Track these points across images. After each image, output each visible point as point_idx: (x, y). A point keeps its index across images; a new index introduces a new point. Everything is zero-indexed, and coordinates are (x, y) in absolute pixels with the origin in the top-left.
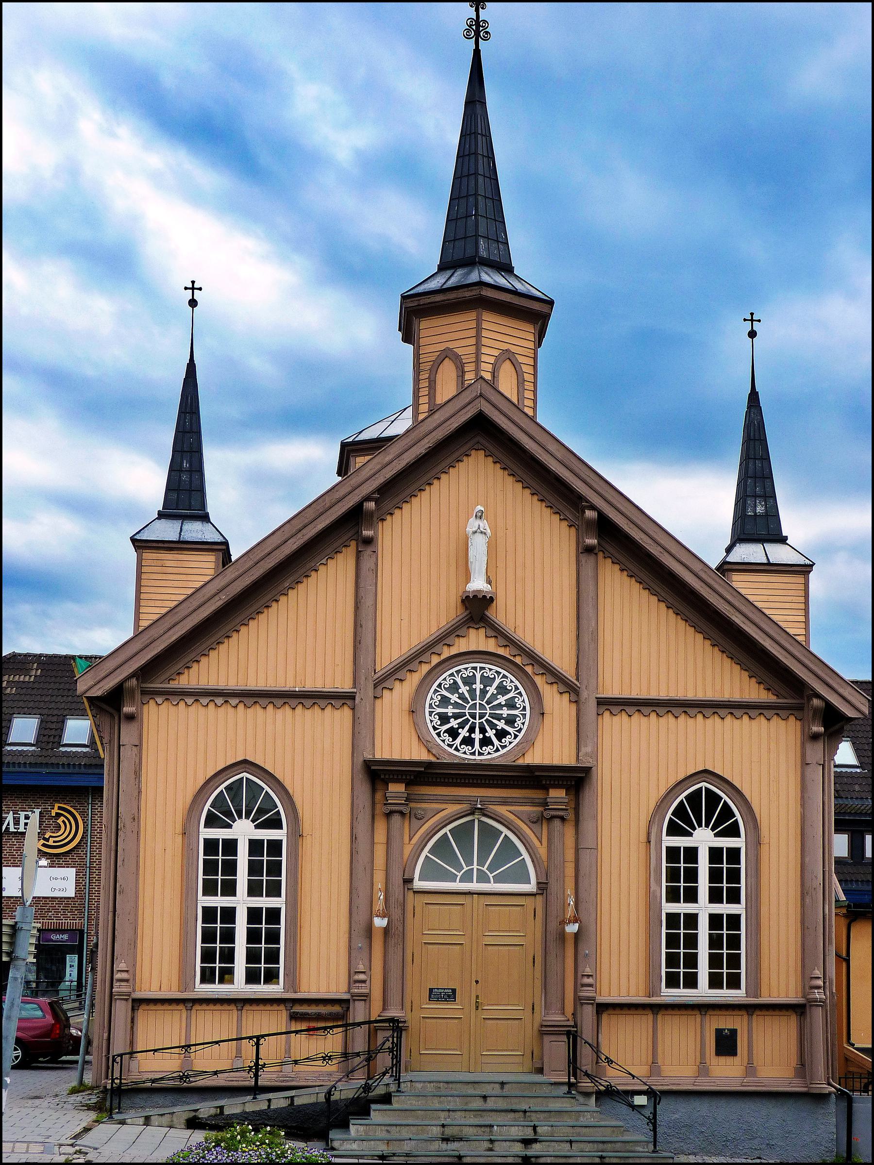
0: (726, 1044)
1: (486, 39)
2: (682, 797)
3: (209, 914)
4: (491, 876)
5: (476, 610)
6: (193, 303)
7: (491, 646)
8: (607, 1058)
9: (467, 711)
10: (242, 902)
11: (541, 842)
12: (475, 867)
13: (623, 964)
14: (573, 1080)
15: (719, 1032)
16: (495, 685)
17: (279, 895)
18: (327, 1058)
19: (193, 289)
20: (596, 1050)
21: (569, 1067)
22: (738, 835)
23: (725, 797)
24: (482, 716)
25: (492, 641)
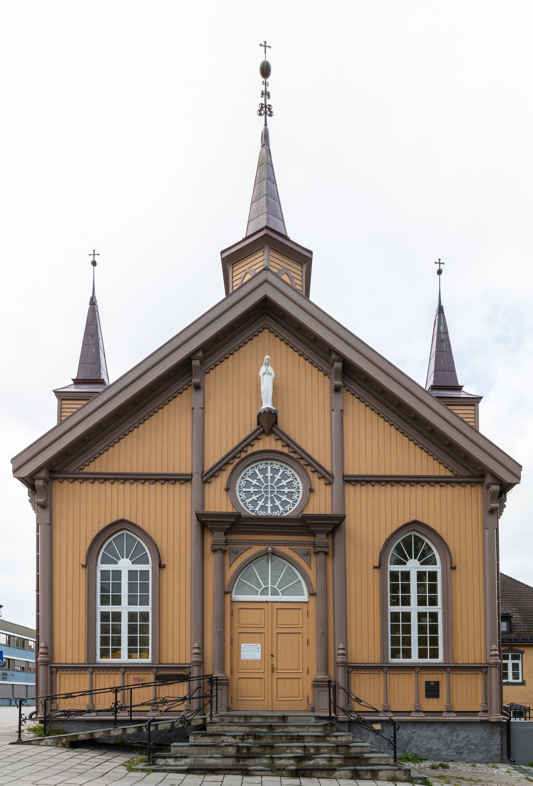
0: (432, 690)
1: (270, 115)
2: (399, 541)
3: (105, 616)
4: (279, 591)
5: (268, 423)
6: (94, 264)
7: (278, 446)
8: (357, 698)
9: (262, 490)
10: (124, 609)
11: (310, 567)
12: (270, 586)
13: (366, 643)
14: (333, 715)
15: (427, 683)
16: (280, 506)
17: (148, 605)
18: (69, 696)
19: (94, 255)
20: (348, 694)
21: (330, 705)
22: (435, 563)
23: (427, 541)
24: (272, 492)
25: (279, 443)
